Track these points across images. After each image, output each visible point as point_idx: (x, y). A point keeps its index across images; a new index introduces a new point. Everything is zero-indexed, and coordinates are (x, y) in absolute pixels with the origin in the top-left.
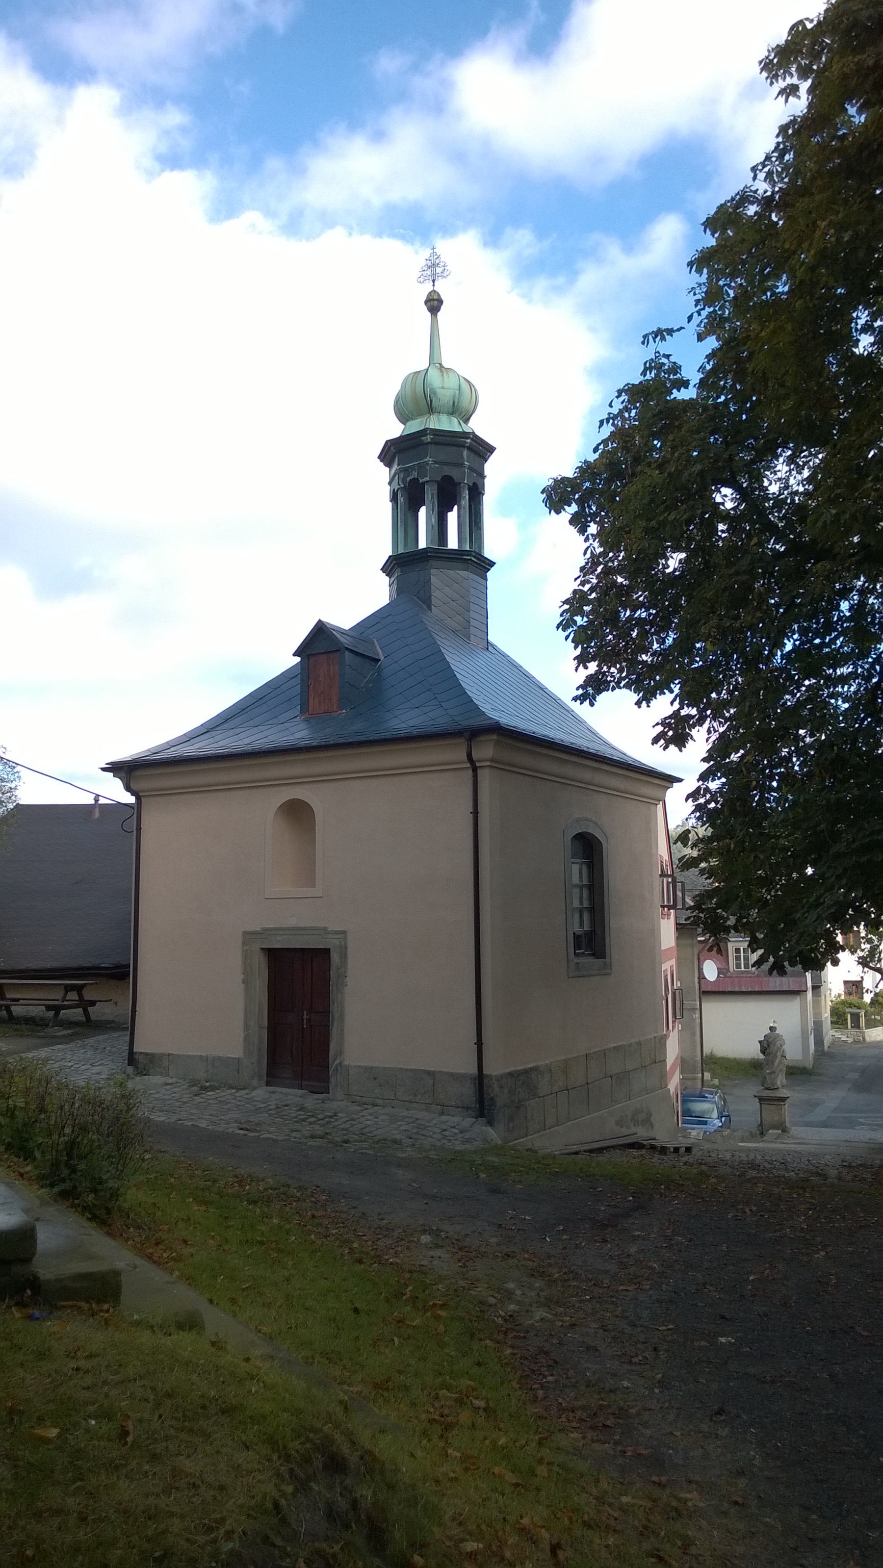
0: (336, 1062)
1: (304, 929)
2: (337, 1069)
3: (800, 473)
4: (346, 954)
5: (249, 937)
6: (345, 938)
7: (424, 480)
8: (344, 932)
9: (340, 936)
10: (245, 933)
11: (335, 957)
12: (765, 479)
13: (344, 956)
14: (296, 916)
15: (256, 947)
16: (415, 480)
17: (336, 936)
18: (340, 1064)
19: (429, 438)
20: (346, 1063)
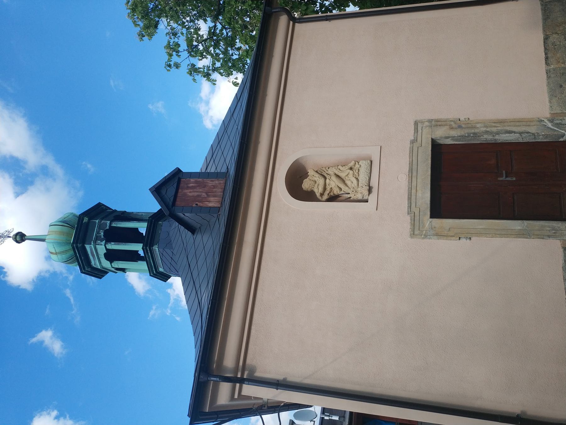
0: (550, 125)
1: (411, 164)
2: (558, 125)
3: (241, 47)
4: (437, 121)
5: (416, 231)
6: (422, 122)
7: (108, 225)
8: (416, 124)
9: (420, 129)
10: (413, 235)
11: (441, 134)
12: (223, 50)
13: (436, 123)
14: (402, 180)
15: (428, 222)
16: (106, 232)
17: (420, 131)
18: (551, 121)
19: (86, 220)
20: (548, 116)
